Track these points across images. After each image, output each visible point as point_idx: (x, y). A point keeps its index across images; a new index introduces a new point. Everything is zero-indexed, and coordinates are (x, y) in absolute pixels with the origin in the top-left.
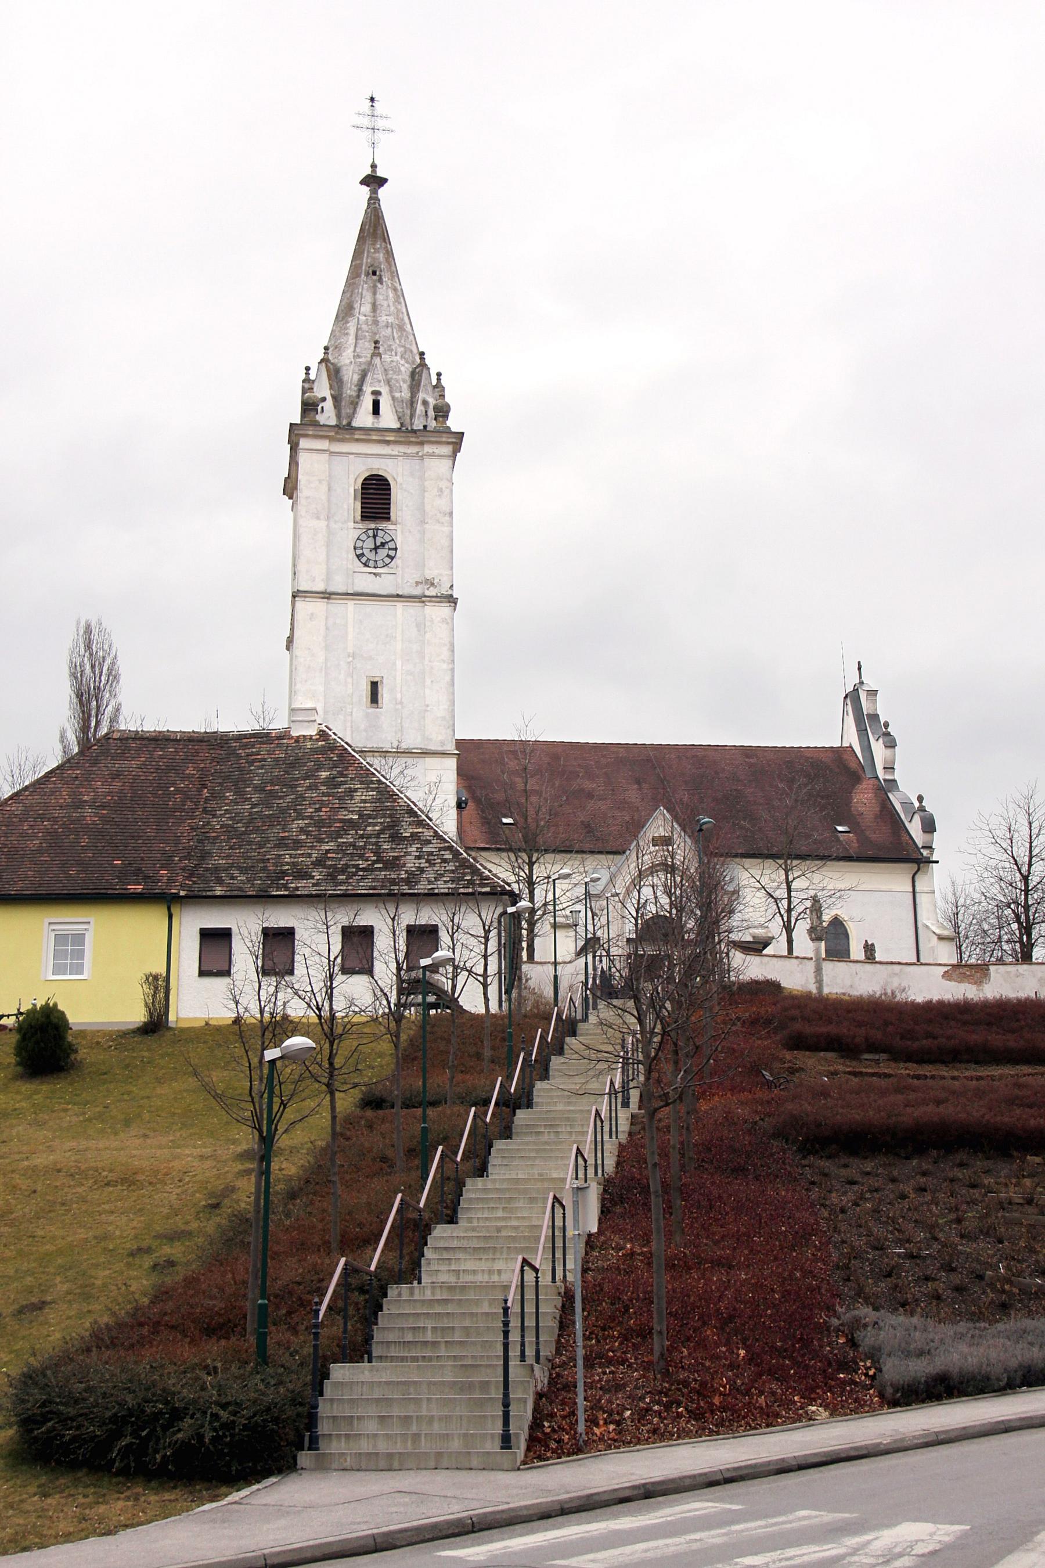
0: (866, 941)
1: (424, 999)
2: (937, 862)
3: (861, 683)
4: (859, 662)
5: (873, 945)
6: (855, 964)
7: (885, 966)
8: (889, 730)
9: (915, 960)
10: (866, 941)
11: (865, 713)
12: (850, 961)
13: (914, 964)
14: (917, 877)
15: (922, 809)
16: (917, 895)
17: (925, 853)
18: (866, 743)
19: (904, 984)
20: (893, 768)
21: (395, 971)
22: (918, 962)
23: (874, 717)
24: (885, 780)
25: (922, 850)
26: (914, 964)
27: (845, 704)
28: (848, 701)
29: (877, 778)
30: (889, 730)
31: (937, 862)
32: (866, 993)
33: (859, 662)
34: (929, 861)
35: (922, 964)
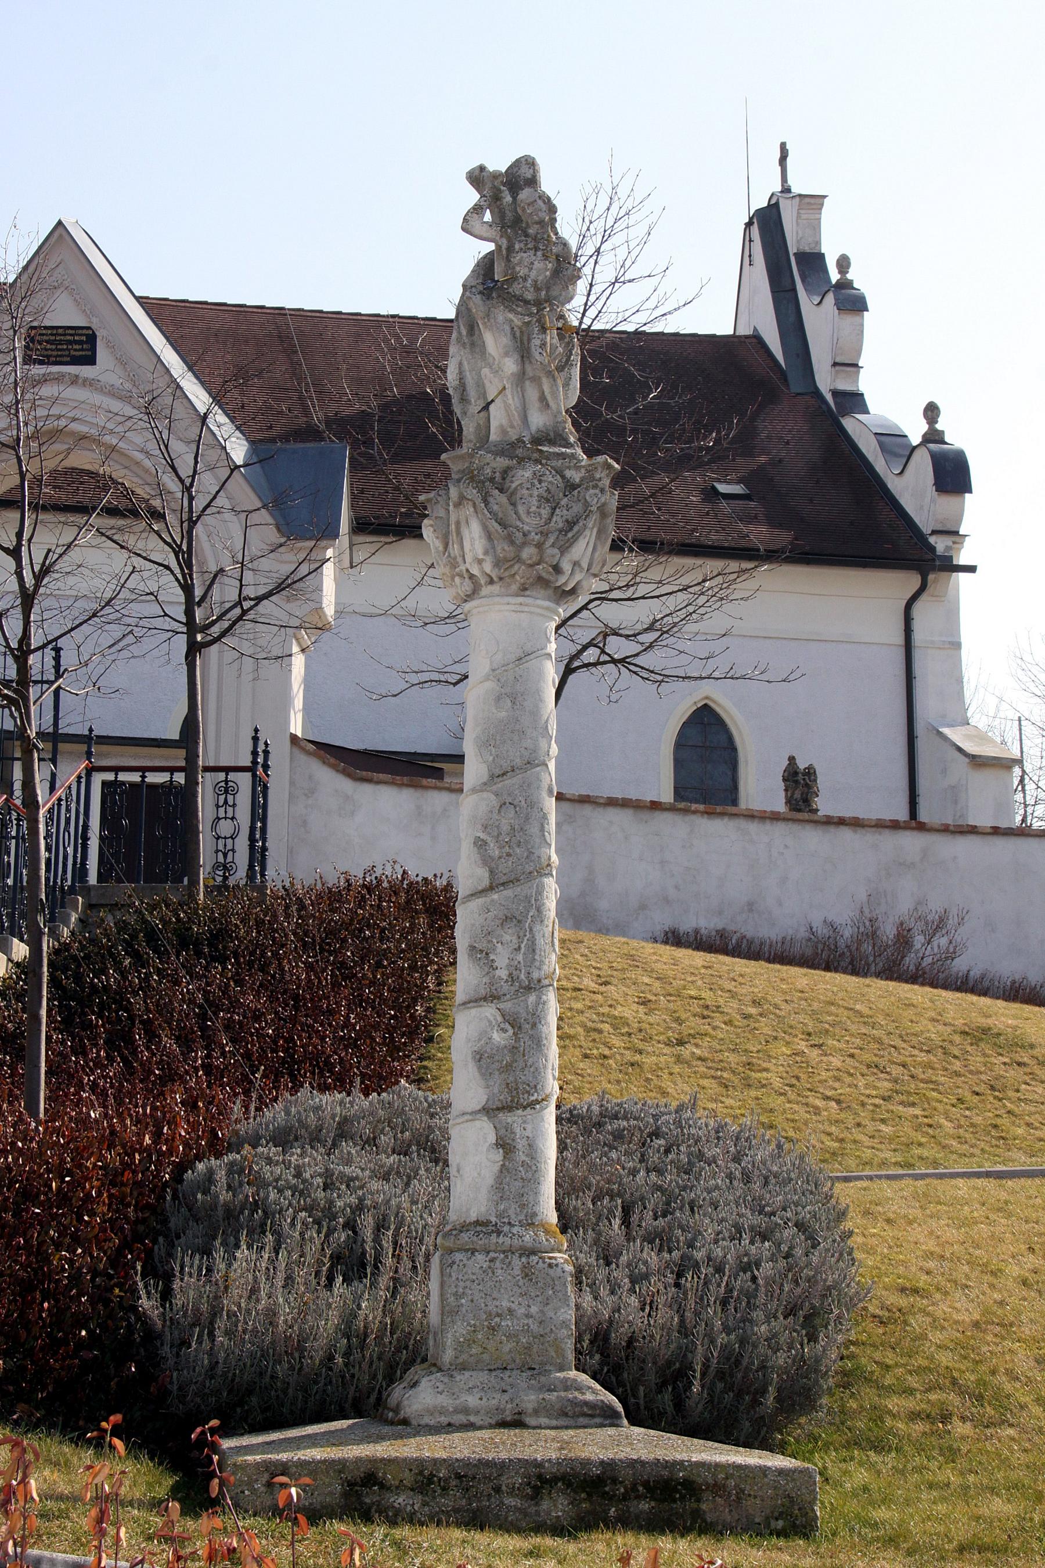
0: (792, 759)
1: (143, 777)
2: (972, 569)
3: (786, 190)
4: (783, 146)
5: (810, 773)
6: (768, 826)
7: (870, 837)
8: (849, 276)
9: (902, 814)
10: (792, 759)
11: (792, 250)
12: (816, 822)
13: (895, 825)
14: (917, 610)
15: (933, 437)
16: (917, 655)
17: (940, 544)
18: (792, 319)
19: (935, 905)
20: (856, 366)
21: (1027, 780)
22: (914, 822)
23: (813, 261)
24: (835, 393)
25: (932, 540)
26: (895, 825)
27: (747, 240)
28: (755, 230)
29: (817, 393)
30: (849, 276)
31: (972, 569)
32: (803, 933)
33: (783, 146)
34: (950, 567)
35: (922, 827)
